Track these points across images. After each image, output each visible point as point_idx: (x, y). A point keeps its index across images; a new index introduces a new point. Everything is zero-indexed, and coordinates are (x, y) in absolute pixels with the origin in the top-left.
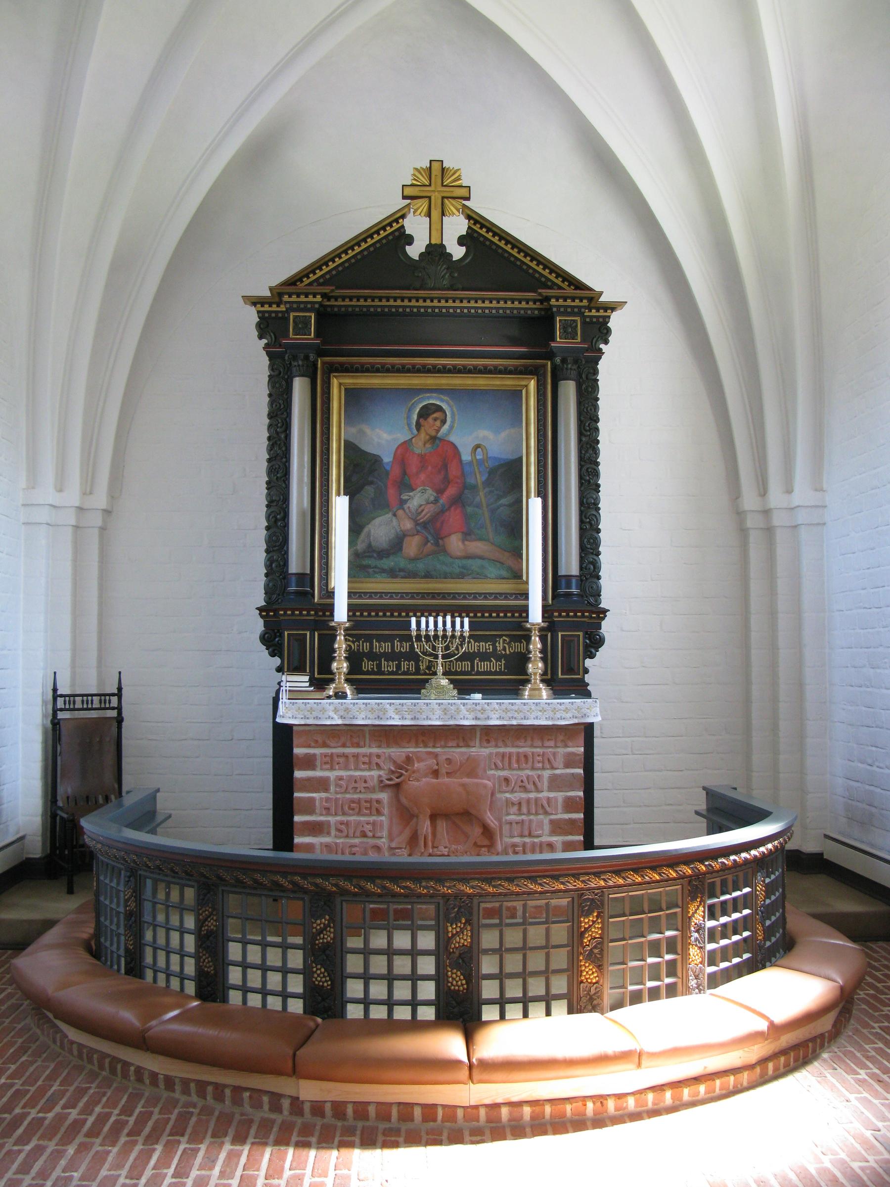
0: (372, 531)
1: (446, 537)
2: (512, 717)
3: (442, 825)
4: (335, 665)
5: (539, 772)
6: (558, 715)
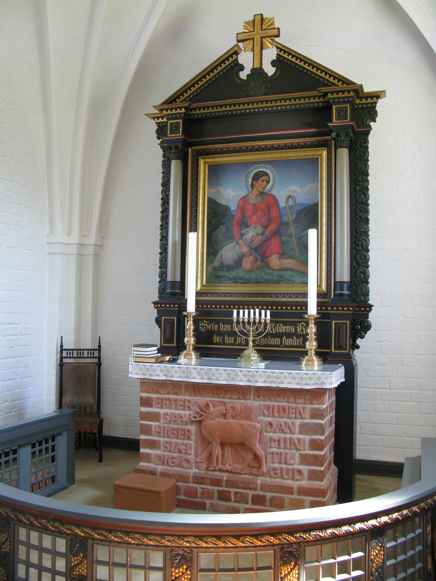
0: (224, 254)
1: (268, 257)
2: (273, 382)
3: (228, 451)
4: (186, 339)
5: (293, 420)
6: (304, 382)
